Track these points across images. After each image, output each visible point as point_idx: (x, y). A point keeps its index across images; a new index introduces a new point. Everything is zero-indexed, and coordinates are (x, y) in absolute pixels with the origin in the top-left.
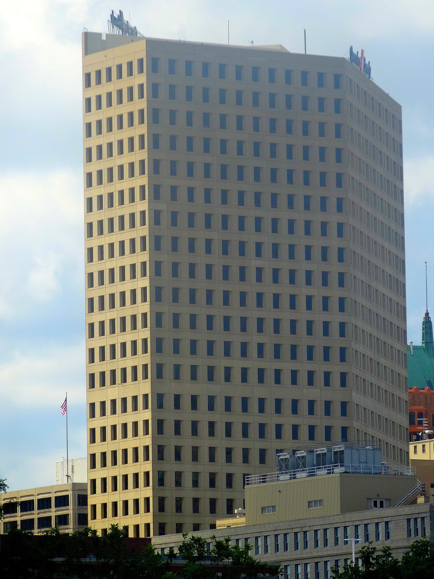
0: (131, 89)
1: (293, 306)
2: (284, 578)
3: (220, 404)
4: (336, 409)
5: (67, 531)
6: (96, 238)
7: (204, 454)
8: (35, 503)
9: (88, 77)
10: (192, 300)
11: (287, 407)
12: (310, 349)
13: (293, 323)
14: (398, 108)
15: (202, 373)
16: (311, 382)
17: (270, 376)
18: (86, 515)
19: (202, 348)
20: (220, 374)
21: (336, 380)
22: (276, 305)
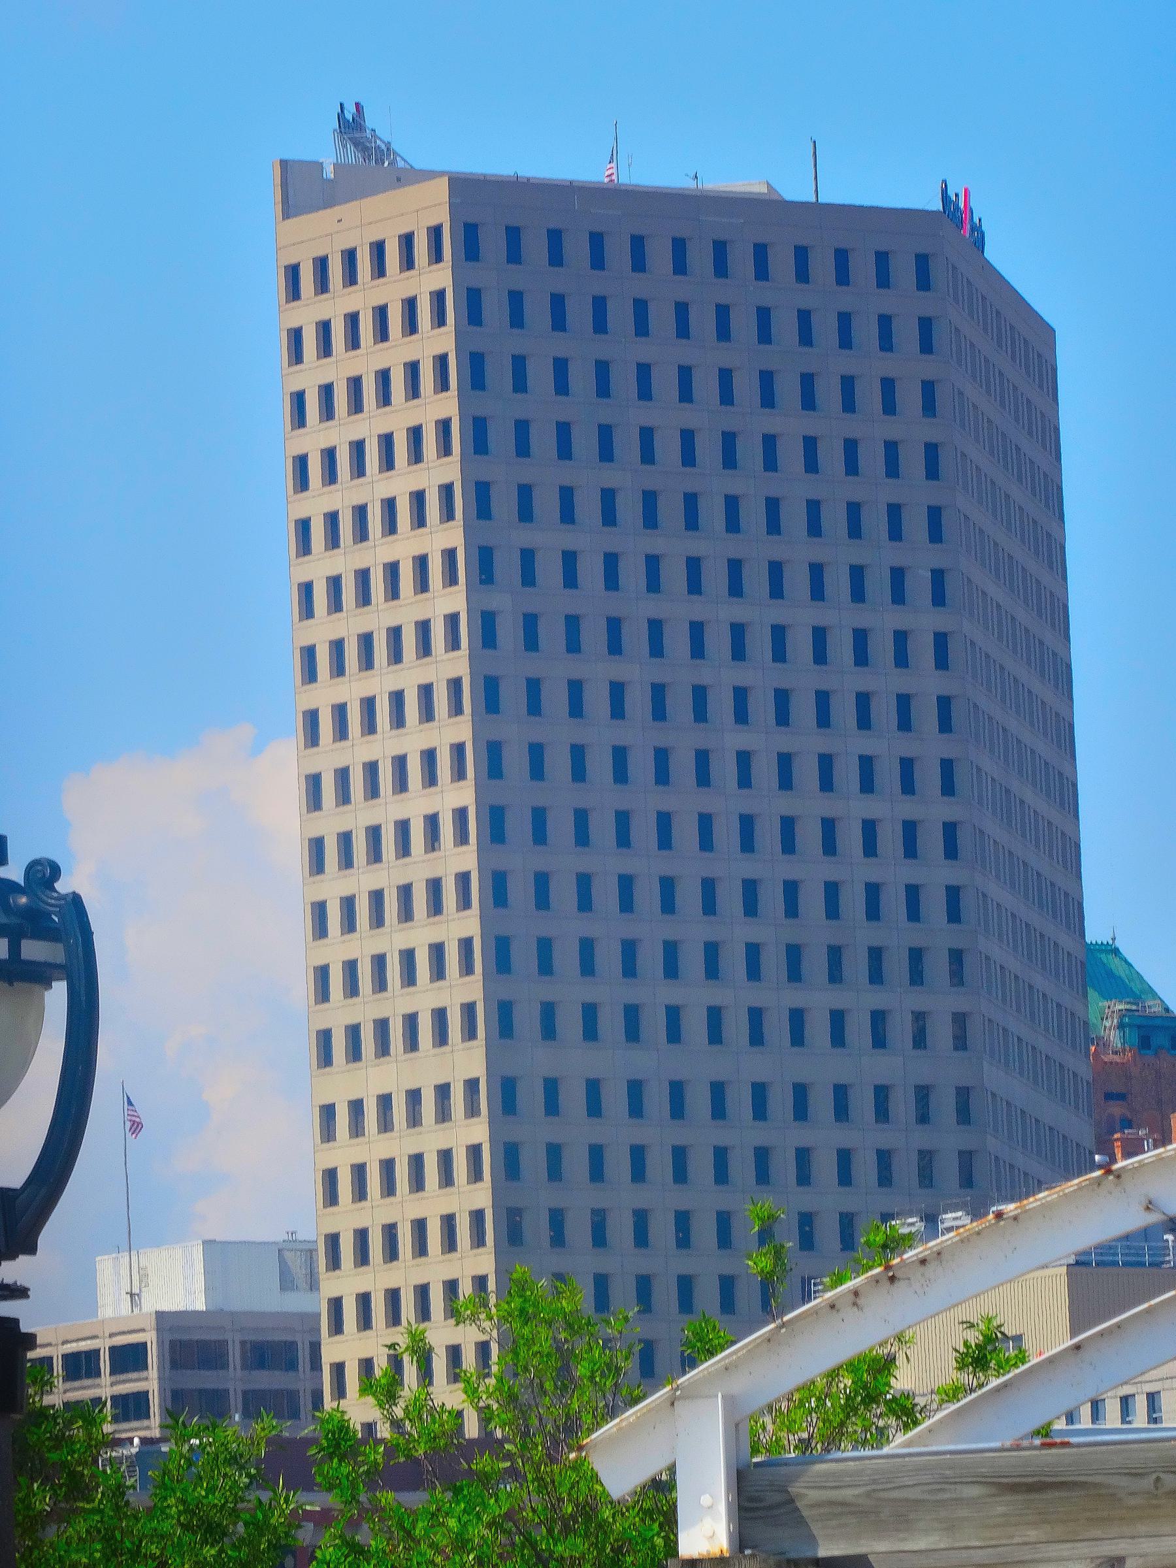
0: (410, 305)
1: (830, 846)
2: (349, 1566)
4: (945, 1105)
7: (621, 1229)
8: (55, 1365)
11: (822, 1103)
13: (832, 890)
14: (1052, 331)
15: (611, 1023)
16: (757, 1037)
20: (654, 1024)
21: (941, 1033)
22: (789, 845)
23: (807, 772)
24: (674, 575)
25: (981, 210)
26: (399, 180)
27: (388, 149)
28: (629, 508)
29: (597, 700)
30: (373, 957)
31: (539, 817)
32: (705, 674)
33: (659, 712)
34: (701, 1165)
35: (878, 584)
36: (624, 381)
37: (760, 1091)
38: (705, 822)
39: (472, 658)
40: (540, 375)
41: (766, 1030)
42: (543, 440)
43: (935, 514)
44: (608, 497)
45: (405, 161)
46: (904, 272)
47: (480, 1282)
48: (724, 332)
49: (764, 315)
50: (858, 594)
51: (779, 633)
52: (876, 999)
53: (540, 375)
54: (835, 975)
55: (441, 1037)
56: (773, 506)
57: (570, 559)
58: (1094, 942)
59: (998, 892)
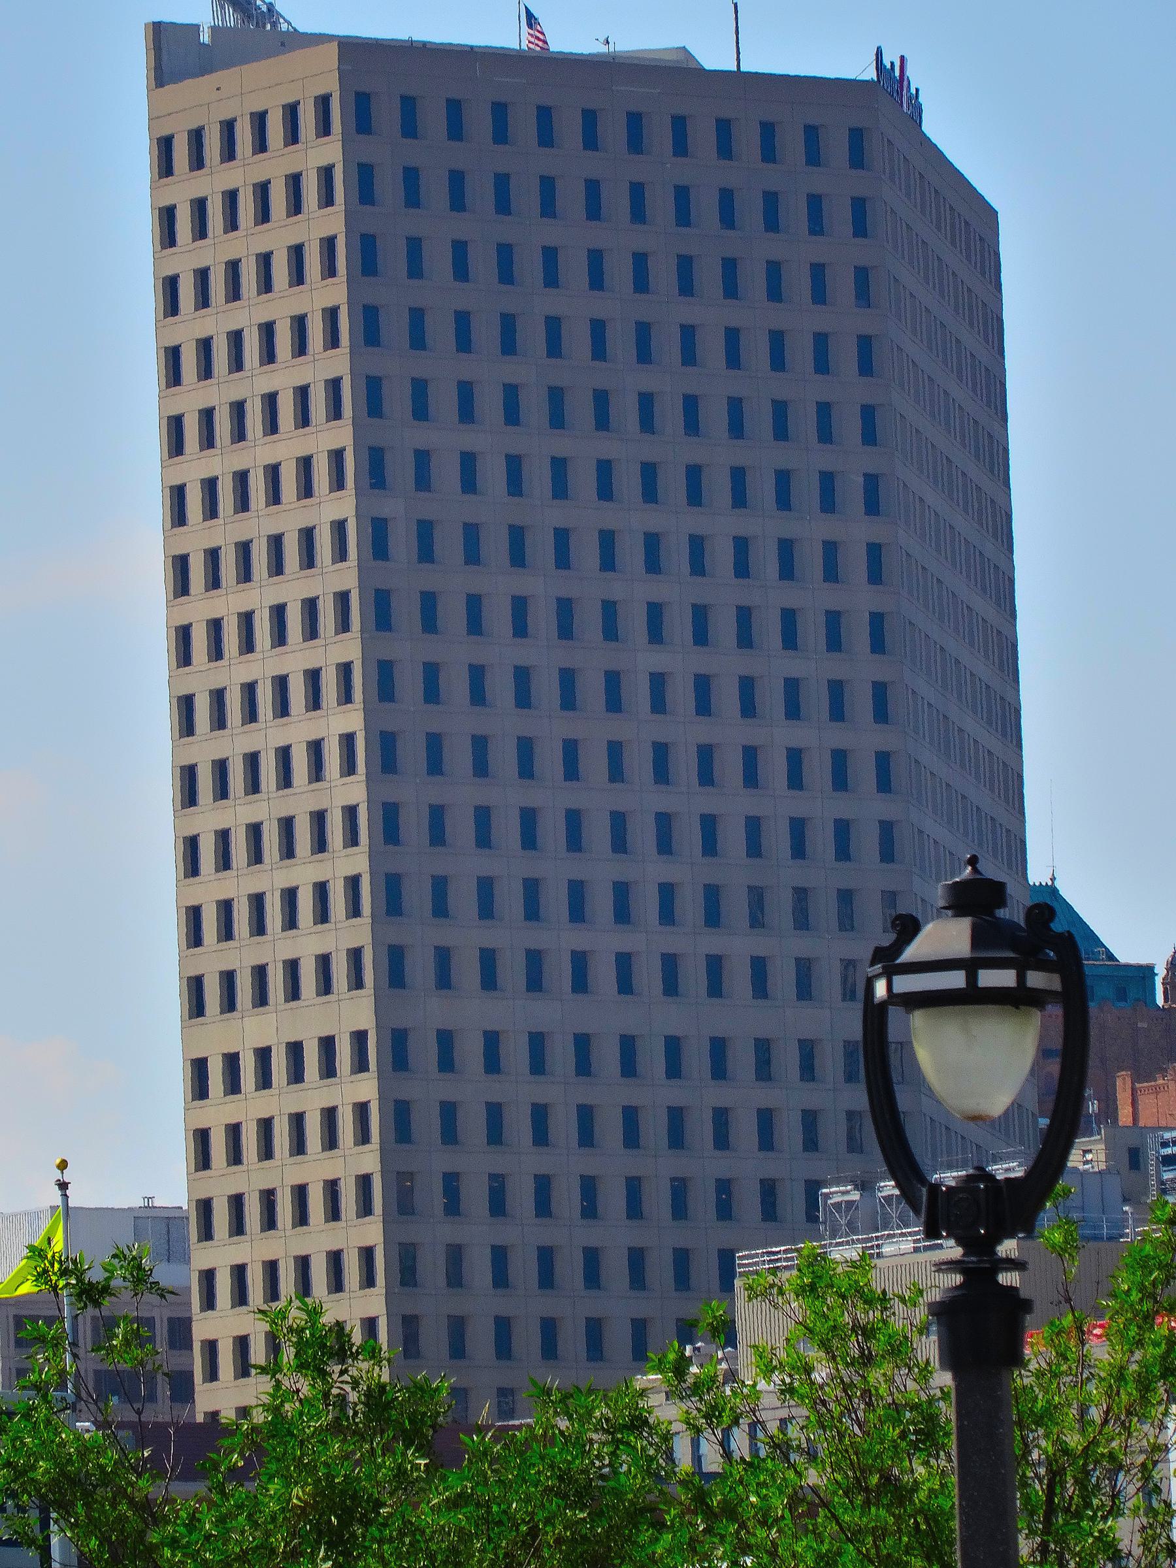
3: (561, 1055)
5: (728, 1352)
6: (201, 597)
9: (165, 146)
10: (526, 770)
12: (757, 898)
14: (995, 213)
15: (512, 971)
17: (694, 977)
18: (190, 1375)
19: (510, 900)
20: (559, 972)
22: (722, 1141)
23: (727, 697)
24: (584, 479)
25: (916, 77)
26: (283, 44)
27: (269, 10)
28: (535, 407)
29: (498, 617)
30: (253, 968)
31: (435, 744)
32: (616, 589)
33: (566, 630)
34: (610, 1128)
35: (807, 491)
36: (526, 196)
37: (673, 1046)
38: (615, 751)
39: (358, 494)
40: (439, 260)
41: (669, 697)
42: (441, 331)
43: (859, 206)
44: (511, 393)
45: (289, 23)
46: (837, 147)
47: (370, 1325)
48: (638, 214)
49: (682, 195)
50: (784, 501)
51: (697, 545)
52: (802, 945)
53: (439, 260)
54: (757, 920)
55: (325, 986)
56: (691, 404)
57: (468, 461)
58: (1037, 884)
59: (935, 829)
